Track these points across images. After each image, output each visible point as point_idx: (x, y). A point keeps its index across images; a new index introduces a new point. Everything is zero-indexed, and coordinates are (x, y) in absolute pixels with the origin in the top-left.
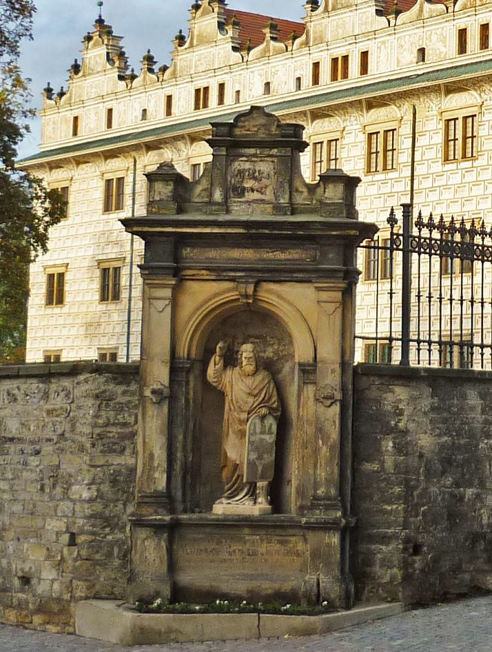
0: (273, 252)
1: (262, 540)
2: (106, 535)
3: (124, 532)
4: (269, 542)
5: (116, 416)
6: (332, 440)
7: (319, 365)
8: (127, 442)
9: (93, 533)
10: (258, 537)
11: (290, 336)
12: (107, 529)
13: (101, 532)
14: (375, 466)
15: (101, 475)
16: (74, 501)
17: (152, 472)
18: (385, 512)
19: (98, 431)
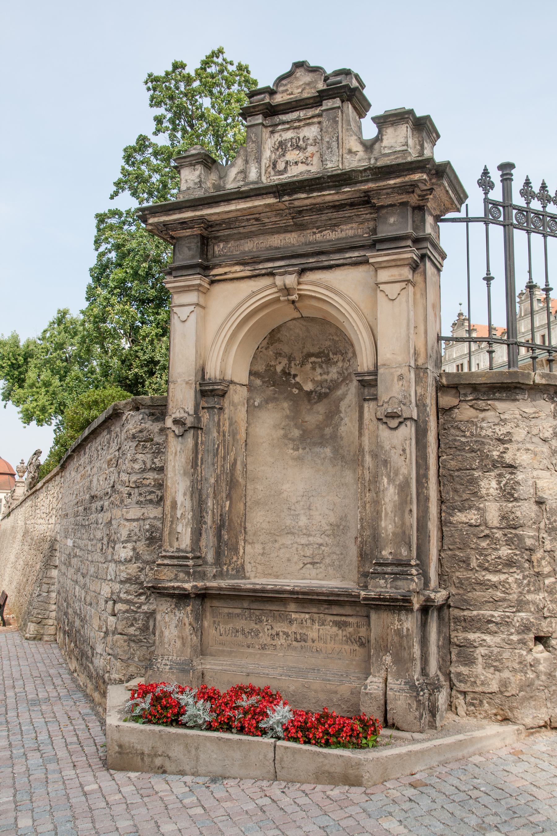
1: (313, 621)
2: (142, 604)
5: (153, 460)
6: (401, 477)
7: (381, 371)
9: (127, 602)
10: (307, 616)
11: (352, 345)
14: (472, 517)
15: (137, 530)
17: (174, 526)
18: (484, 585)
19: (134, 478)
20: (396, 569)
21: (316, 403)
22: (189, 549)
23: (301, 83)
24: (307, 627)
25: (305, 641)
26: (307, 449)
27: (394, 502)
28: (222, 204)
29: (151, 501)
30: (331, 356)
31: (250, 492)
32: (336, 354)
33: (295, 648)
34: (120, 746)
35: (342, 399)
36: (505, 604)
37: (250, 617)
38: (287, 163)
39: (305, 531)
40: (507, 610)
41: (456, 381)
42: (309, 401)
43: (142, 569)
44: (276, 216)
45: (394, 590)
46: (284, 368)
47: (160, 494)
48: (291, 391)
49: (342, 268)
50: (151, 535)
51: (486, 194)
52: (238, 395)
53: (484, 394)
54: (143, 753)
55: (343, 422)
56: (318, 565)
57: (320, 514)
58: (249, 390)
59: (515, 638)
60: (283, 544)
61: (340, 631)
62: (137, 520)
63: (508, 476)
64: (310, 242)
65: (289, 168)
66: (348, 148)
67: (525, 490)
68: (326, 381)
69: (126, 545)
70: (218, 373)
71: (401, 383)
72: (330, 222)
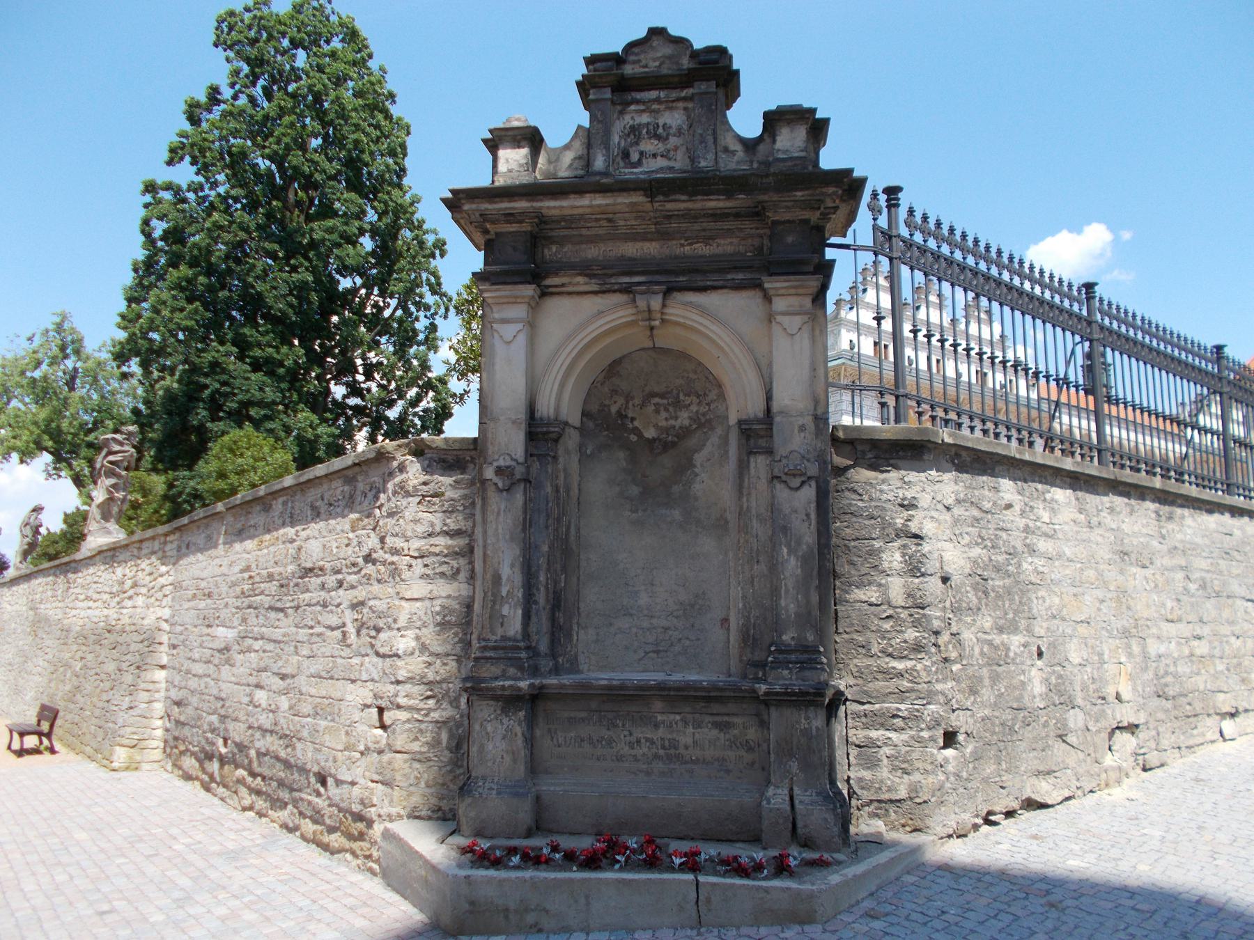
1: (686, 723)
2: (430, 710)
4: (698, 726)
9: (409, 709)
10: (678, 717)
11: (720, 386)
14: (872, 594)
15: (421, 613)
17: (497, 607)
22: (519, 637)
23: (659, 55)
29: (443, 574)
30: (682, 397)
31: (583, 564)
34: (472, 903)
36: (913, 695)
38: (641, 153)
39: (646, 612)
41: (855, 435)
44: (636, 218)
45: (801, 682)
49: (720, 291)
51: (875, 219)
52: (571, 440)
54: (507, 910)
55: (698, 479)
58: (582, 435)
59: (925, 734)
67: (931, 566)
68: (674, 427)
70: (552, 411)
71: (802, 435)
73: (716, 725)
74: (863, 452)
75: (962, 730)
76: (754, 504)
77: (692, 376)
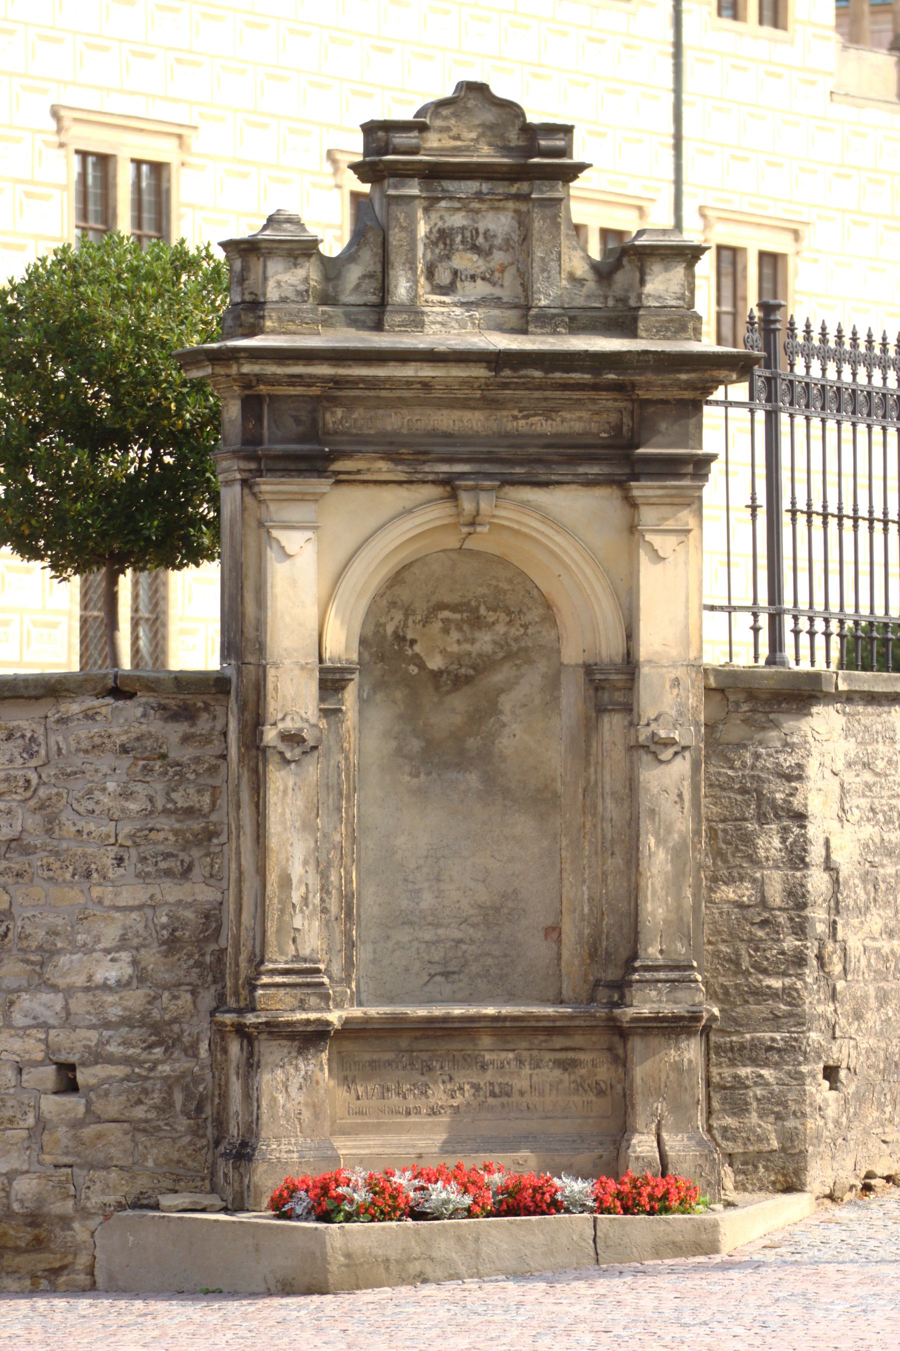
0: (526, 417)
1: (520, 1062)
3: (196, 1056)
4: (537, 1065)
6: (676, 836)
8: (196, 853)
9: (127, 1061)
10: (511, 1055)
12: (157, 1050)
13: (144, 1056)
15: (140, 927)
16: (69, 992)
17: (287, 918)
18: (760, 994)
20: (673, 975)
21: (449, 692)
24: (512, 1073)
25: (508, 1095)
26: (434, 775)
27: (666, 873)
28: (392, 363)
29: (168, 873)
30: (483, 611)
32: (495, 610)
33: (492, 1108)
34: (348, 1256)
35: (501, 691)
37: (412, 1064)
38: (455, 273)
39: (430, 919)
40: (793, 1029)
42: (437, 688)
43: (155, 998)
46: (397, 627)
47: (187, 859)
48: (407, 671)
49: (566, 487)
50: (172, 934)
53: (766, 703)
54: (388, 1260)
55: (506, 731)
56: (456, 976)
57: (459, 889)
60: (397, 943)
61: (566, 1075)
62: (140, 908)
63: (796, 830)
64: (506, 432)
65: (458, 284)
66: (568, 269)
68: (469, 654)
69: (117, 955)
71: (675, 691)
72: (544, 404)
73: (559, 1064)
74: (737, 704)
75: (844, 1065)
76: (607, 778)
77: (504, 585)
